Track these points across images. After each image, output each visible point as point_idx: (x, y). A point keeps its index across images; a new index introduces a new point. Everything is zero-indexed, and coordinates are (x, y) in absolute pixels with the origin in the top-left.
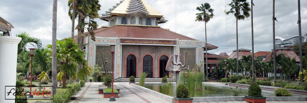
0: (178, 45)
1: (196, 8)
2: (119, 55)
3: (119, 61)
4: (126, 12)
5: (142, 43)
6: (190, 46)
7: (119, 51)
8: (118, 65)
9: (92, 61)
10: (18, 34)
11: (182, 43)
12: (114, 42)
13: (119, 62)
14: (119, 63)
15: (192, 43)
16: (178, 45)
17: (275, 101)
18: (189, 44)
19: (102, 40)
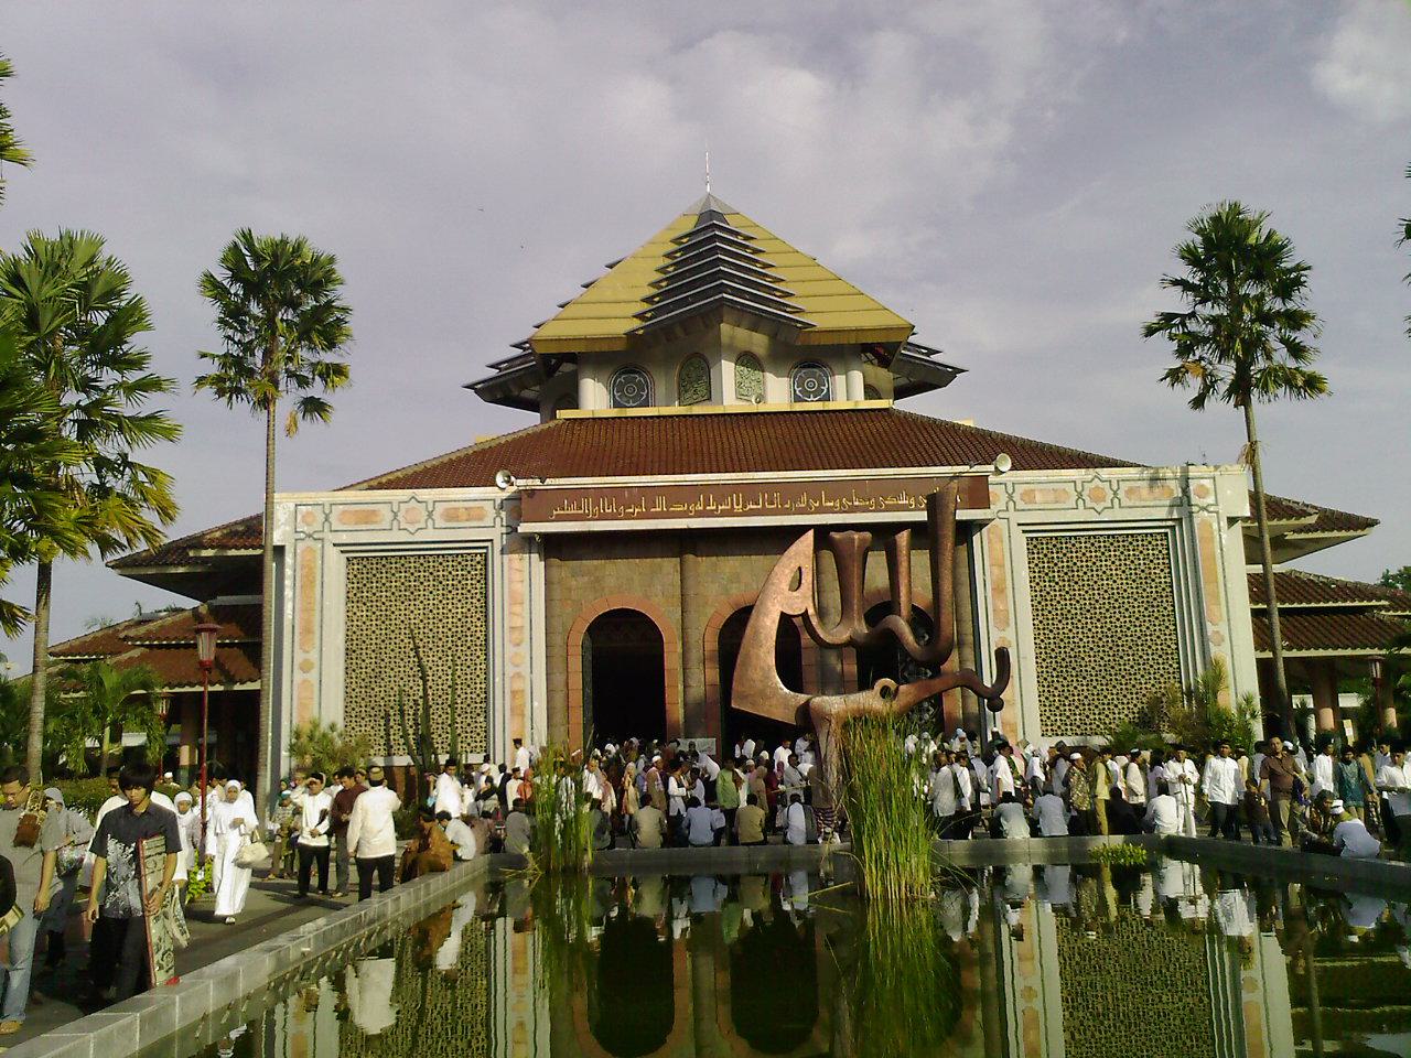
0: (1011, 514)
1: (185, 436)
2: (518, 622)
3: (525, 670)
4: (637, 323)
5: (699, 515)
6: (1119, 514)
7: (518, 587)
8: (514, 693)
9: (313, 676)
10: (512, 343)
11: (1038, 497)
12: (480, 518)
13: (519, 675)
14: (518, 685)
15: (1130, 492)
16: (1011, 514)
17: (526, 953)
18: (1098, 500)
19: (385, 511)
